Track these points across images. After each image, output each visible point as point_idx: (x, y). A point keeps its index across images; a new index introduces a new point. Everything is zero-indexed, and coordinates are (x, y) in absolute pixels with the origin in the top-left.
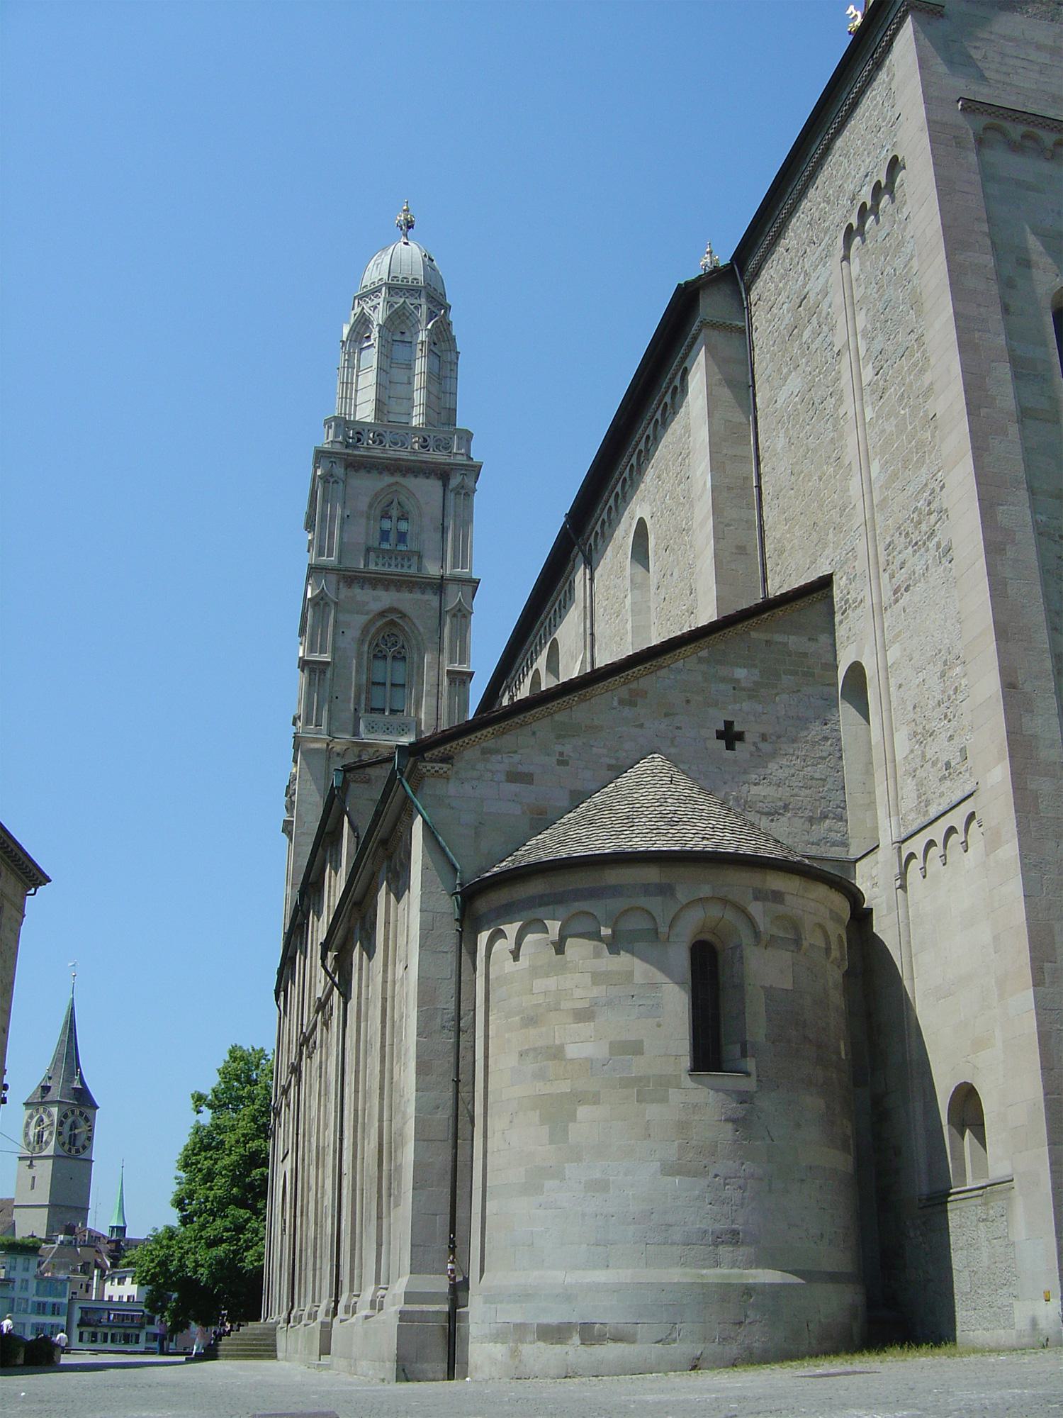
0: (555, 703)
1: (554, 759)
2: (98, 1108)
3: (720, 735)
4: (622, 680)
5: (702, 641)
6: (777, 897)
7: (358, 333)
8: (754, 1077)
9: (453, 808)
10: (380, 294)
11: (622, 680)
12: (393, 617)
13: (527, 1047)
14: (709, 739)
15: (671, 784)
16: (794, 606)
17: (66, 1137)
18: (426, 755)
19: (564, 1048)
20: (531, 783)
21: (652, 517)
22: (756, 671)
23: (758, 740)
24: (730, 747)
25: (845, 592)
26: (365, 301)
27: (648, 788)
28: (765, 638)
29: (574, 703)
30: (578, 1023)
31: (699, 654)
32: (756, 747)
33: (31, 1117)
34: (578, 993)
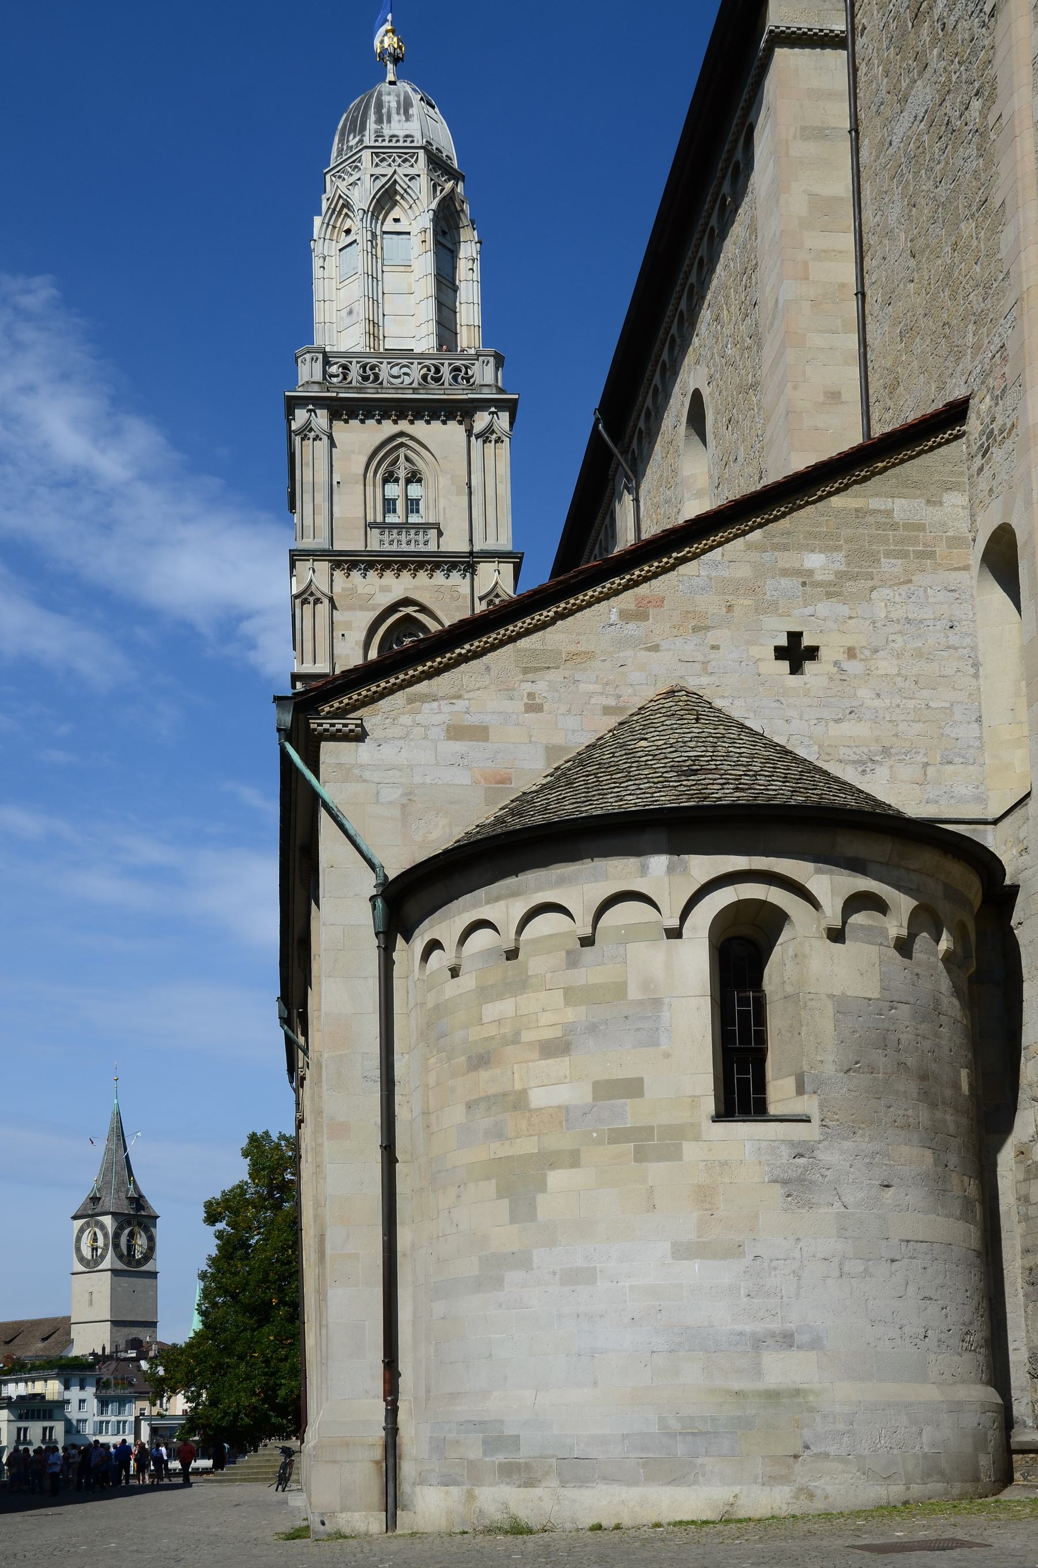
1: (520, 706)
3: (780, 653)
7: (334, 227)
9: (365, 781)
10: (359, 164)
15: (697, 722)
19: (527, 1093)
20: (486, 739)
21: (709, 383)
22: (840, 556)
23: (841, 657)
24: (796, 669)
25: (987, 420)
26: (340, 177)
27: (656, 731)
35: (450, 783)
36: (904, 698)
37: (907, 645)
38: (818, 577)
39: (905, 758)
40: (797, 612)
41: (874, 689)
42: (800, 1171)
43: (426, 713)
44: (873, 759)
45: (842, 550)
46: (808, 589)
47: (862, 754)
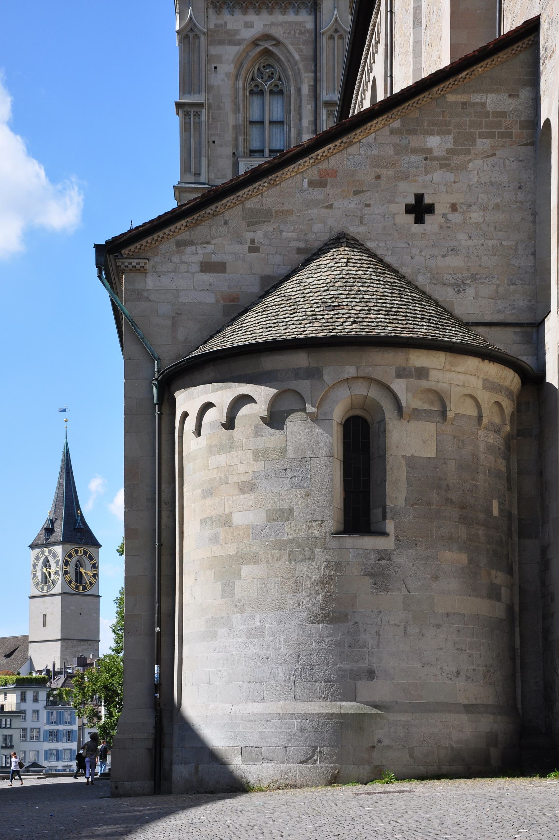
0: (246, 190)
1: (246, 247)
2: (101, 546)
4: (312, 161)
5: (395, 111)
8: (392, 537)
9: (150, 301)
11: (312, 161)
13: (205, 517)
15: (347, 266)
16: (496, 60)
17: (72, 575)
18: (123, 252)
20: (224, 271)
22: (450, 138)
23: (447, 210)
24: (419, 220)
28: (462, 100)
29: (265, 189)
30: (242, 494)
31: (391, 125)
33: (37, 558)
35: (202, 302)
36: (487, 239)
37: (490, 201)
38: (435, 154)
39: (485, 281)
40: (420, 179)
41: (467, 233)
42: (381, 568)
43: (188, 254)
44: (465, 282)
46: (428, 162)
47: (458, 279)
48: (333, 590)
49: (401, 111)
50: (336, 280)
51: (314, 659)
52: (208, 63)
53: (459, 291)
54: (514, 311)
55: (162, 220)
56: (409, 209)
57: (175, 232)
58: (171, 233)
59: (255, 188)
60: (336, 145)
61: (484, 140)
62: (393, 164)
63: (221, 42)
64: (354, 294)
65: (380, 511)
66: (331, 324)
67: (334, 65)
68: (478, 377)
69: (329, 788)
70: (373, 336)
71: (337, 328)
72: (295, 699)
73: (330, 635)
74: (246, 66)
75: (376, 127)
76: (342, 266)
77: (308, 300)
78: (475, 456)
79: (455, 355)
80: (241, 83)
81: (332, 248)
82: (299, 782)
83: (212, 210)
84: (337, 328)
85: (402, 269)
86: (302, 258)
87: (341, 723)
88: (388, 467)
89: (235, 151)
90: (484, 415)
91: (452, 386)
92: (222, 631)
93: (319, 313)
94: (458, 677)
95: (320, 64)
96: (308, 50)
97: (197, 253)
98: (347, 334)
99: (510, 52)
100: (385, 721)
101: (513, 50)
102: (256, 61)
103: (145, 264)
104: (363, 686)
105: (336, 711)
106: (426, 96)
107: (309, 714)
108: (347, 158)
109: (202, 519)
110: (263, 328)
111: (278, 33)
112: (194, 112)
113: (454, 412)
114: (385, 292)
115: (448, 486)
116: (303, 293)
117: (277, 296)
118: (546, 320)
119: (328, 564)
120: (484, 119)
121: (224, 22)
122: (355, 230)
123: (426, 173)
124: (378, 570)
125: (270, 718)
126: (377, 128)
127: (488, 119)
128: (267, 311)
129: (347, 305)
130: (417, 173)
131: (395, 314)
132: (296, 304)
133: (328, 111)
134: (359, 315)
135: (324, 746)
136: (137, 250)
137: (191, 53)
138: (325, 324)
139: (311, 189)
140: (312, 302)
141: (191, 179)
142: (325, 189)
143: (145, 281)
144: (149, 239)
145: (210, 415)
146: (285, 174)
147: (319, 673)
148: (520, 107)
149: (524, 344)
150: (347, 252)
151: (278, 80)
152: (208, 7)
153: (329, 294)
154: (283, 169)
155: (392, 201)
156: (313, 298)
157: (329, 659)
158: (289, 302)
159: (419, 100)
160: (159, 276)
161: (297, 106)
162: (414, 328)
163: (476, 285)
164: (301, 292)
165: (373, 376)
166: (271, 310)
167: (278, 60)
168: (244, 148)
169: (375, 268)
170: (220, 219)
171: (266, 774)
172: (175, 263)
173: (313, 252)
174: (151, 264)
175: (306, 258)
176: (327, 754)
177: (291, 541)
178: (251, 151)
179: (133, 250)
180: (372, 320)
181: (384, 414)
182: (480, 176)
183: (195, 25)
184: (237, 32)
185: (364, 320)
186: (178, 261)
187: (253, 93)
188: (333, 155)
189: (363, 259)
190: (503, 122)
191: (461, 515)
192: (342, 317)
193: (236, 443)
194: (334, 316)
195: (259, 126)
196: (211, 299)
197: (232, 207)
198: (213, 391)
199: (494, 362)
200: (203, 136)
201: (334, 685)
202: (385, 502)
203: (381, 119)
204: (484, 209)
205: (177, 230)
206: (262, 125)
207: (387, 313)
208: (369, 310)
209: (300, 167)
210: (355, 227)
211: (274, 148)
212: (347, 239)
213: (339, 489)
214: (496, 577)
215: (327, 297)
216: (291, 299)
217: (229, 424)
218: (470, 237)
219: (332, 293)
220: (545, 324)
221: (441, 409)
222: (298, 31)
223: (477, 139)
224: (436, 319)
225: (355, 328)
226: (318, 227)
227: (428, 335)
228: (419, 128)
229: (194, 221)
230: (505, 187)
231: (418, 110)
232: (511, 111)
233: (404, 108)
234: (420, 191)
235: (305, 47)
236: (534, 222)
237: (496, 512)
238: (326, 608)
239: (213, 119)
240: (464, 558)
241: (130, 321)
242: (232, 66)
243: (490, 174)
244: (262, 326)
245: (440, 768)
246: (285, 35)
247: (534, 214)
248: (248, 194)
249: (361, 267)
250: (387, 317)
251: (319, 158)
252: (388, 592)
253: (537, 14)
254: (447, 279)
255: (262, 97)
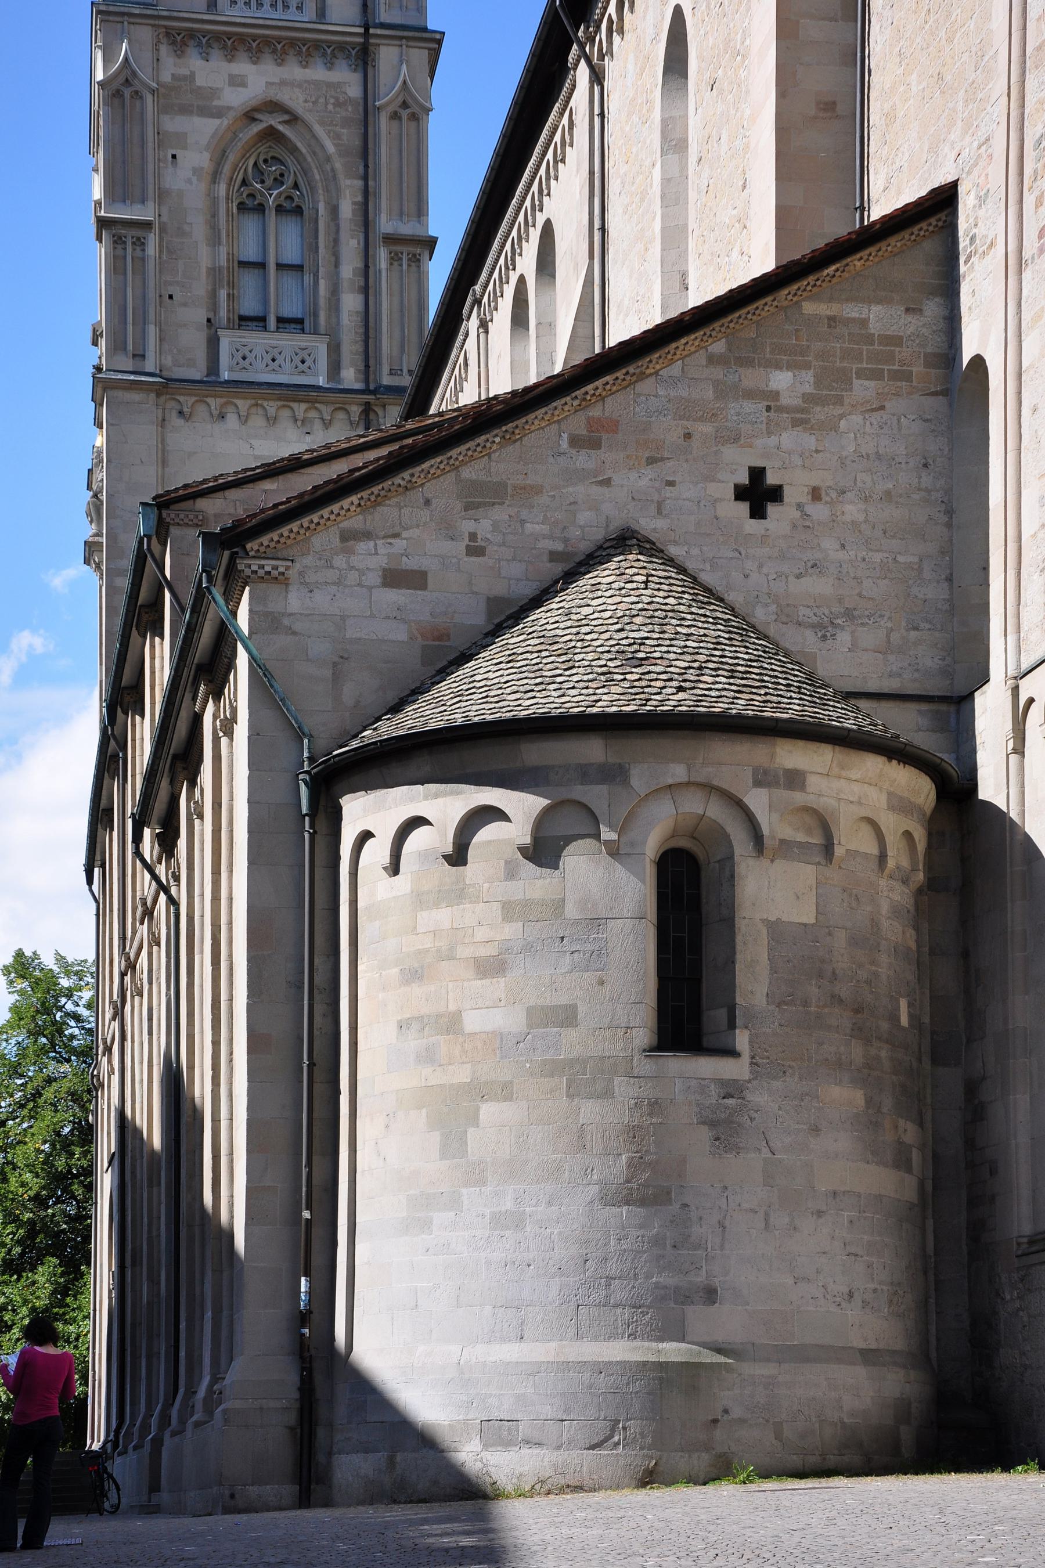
0: (462, 448)
1: (462, 546)
5: (716, 325)
6: (795, 779)
8: (746, 1058)
9: (294, 633)
11: (576, 403)
12: (274, 121)
13: (408, 1016)
14: (721, 500)
15: (646, 588)
16: (884, 249)
18: (249, 546)
20: (424, 586)
22: (808, 376)
23: (805, 499)
24: (758, 513)
28: (828, 313)
29: (495, 447)
32: (802, 511)
34: (482, 934)
35: (386, 638)
36: (871, 550)
38: (785, 401)
40: (759, 442)
41: (839, 538)
42: (728, 1112)
43: (361, 554)
45: (810, 369)
46: (772, 414)
47: (823, 616)
48: (645, 1149)
49: (726, 325)
50: (634, 612)
51: (614, 1268)
52: (159, 147)
53: (824, 638)
54: (916, 675)
55: (319, 493)
56: (741, 493)
57: (339, 514)
58: (333, 517)
59: (479, 445)
60: (617, 378)
61: (867, 383)
62: (713, 414)
63: (185, 110)
64: (671, 640)
65: (722, 1014)
66: (641, 690)
67: (401, 167)
68: (881, 789)
69: (644, 1491)
70: (719, 715)
71: (653, 697)
72: (578, 1336)
73: (641, 1226)
74: (232, 158)
75: (684, 350)
76: (638, 589)
77: (589, 646)
78: (875, 924)
79: (847, 750)
80: (222, 189)
81: (614, 555)
82: (588, 1483)
83: (403, 479)
84: (653, 697)
85: (729, 595)
86: (559, 569)
87: (661, 1379)
88: (739, 939)
89: (211, 316)
90: (889, 854)
91: (842, 803)
92: (441, 1218)
93: (616, 670)
94: (850, 1302)
95: (375, 163)
96: (351, 137)
97: (376, 554)
98: (673, 710)
99: (907, 236)
100: (735, 1375)
101: (912, 234)
102: (250, 150)
103: (287, 568)
104: (696, 1314)
105: (652, 1358)
106: (769, 303)
107: (606, 1363)
108: (635, 401)
109: (401, 1020)
110: (517, 692)
111: (295, 100)
112: (133, 237)
113: (845, 848)
114: (719, 636)
115: (834, 973)
116: (578, 633)
117: (528, 634)
118: (976, 694)
119: (636, 1103)
120: (865, 347)
121: (191, 71)
122: (648, 525)
123: (768, 433)
124: (723, 1116)
125: (536, 1370)
126: (685, 353)
127: (871, 348)
128: (518, 661)
129: (661, 658)
130: (753, 433)
131: (744, 676)
132: (569, 651)
133: (390, 253)
134: (686, 677)
135: (631, 1419)
136: (272, 545)
137: (128, 126)
138: (630, 690)
139: (574, 451)
140: (599, 649)
141: (128, 364)
142: (598, 452)
143: (286, 597)
144: (295, 526)
145: (417, 839)
146: (530, 423)
147: (620, 1292)
148: (924, 330)
149: (936, 732)
150: (642, 564)
151: (293, 188)
152: (159, 42)
153: (627, 638)
154: (526, 415)
155: (710, 478)
156: (599, 643)
157: (639, 1268)
158: (556, 647)
159: (757, 308)
160: (311, 591)
161: (331, 239)
162: (779, 703)
163: (854, 627)
164: (574, 630)
165: (715, 782)
166: (524, 659)
167: (294, 150)
168: (229, 311)
169: (694, 594)
170: (417, 496)
171: (527, 1468)
172: (338, 569)
173: (577, 560)
174: (296, 570)
175: (566, 569)
176: (636, 1432)
177: (572, 1062)
178: (242, 318)
179: (265, 543)
180: (709, 686)
181: (732, 847)
182: (859, 442)
183: (134, 73)
184: (214, 93)
185: (696, 685)
186: (344, 566)
187: (244, 209)
188: (610, 395)
189: (670, 577)
190: (897, 353)
191: (854, 1024)
192: (657, 680)
193: (471, 890)
194: (643, 677)
195: (256, 271)
196: (400, 634)
197: (438, 477)
198: (426, 798)
199: (905, 763)
200: (151, 283)
201: (648, 1313)
202: (734, 998)
203: (693, 337)
204: (866, 500)
205: (343, 513)
206: (261, 270)
207: (730, 674)
208: (700, 668)
209: (557, 412)
210: (648, 520)
211: (285, 316)
212: (638, 540)
213: (653, 974)
214: (905, 1130)
215: (624, 642)
216: (557, 642)
217: (458, 857)
218: (843, 546)
219: (632, 635)
220: (976, 700)
221: (824, 842)
222: (332, 101)
223: (854, 380)
224: (809, 687)
225: (685, 700)
226: (584, 517)
227: (806, 715)
228: (756, 357)
229: (373, 498)
230: (900, 463)
231: (754, 325)
232: (910, 336)
233: (731, 321)
234: (759, 463)
235: (345, 131)
236: (949, 525)
237: (904, 1021)
238: (633, 1178)
239: (169, 252)
240: (858, 1097)
241: (260, 668)
242: (207, 156)
243: (876, 439)
244: (515, 688)
245: (824, 1459)
246: (306, 105)
247: (948, 512)
248: (466, 455)
249: (671, 591)
250: (731, 681)
251: (588, 398)
252: (738, 1153)
253: (950, 179)
254: (804, 616)
255: (261, 216)
